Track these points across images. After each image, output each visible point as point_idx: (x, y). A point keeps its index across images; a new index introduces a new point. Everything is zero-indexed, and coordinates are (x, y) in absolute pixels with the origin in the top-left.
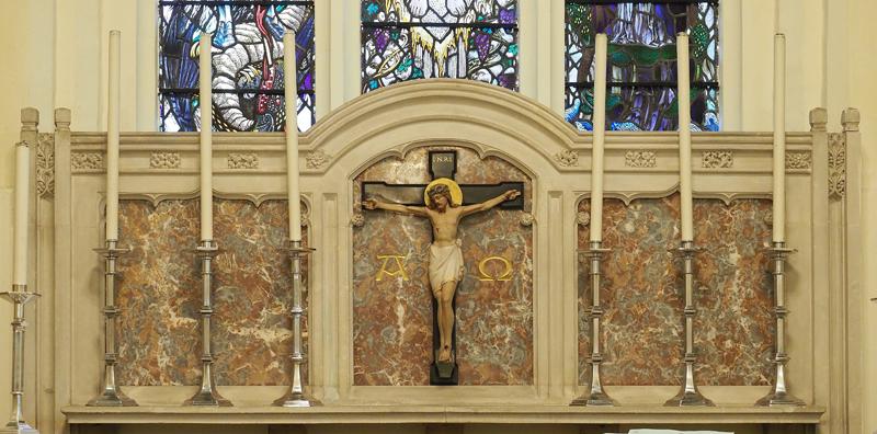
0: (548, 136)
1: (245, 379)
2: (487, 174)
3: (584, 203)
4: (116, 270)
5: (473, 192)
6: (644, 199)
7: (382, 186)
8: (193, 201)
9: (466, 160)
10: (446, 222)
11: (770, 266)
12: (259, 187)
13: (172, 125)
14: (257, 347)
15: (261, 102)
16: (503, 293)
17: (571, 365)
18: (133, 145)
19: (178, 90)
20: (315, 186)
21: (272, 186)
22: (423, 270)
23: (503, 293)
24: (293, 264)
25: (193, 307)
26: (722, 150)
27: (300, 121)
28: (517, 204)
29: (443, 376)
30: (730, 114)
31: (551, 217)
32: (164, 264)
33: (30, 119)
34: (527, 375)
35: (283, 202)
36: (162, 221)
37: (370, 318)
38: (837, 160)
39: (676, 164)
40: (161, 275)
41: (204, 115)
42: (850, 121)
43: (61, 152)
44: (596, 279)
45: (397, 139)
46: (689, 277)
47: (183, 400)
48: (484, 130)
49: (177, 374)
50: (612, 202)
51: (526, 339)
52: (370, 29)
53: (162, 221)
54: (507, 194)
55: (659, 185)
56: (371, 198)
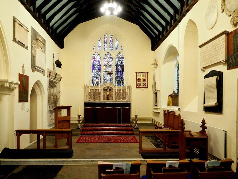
0: (204, 46)
1: (97, 99)
2: (110, 88)
3: (116, 90)
4: (89, 93)
5: (110, 89)
6: (119, 90)
7: (212, 26)
8: (94, 90)
9: (109, 87)
10: (108, 91)
11: (126, 94)
12: (98, 89)
13: (92, 85)
14: (97, 98)
15: (98, 83)
16: (111, 95)
17: (115, 99)
18: (91, 86)
19: (93, 83)
20: (101, 89)
21: (99, 89)
22: (107, 93)
23: (111, 95)
24: (99, 93)
25: (94, 96)
26: (124, 87)
27: (100, 85)
28: (112, 90)
29: (108, 99)
30: (125, 84)
31: (114, 91)
32: (92, 93)
33: (85, 85)
34: (113, 99)
35: (99, 90)
36: (92, 91)
37: (104, 96)
38: (130, 88)
39: (121, 88)
40: (92, 94)
41: (94, 85)
42: (131, 85)
43: (86, 87)
44: (117, 94)
45: (106, 86)
46: (122, 94)
47: (42, 53)
48: (110, 86)
49: (93, 99)
50: (117, 90)
51: (113, 97)
52: (104, 79)
53: (92, 91)
54: (111, 89)
55: (120, 89)
56: (104, 89)
